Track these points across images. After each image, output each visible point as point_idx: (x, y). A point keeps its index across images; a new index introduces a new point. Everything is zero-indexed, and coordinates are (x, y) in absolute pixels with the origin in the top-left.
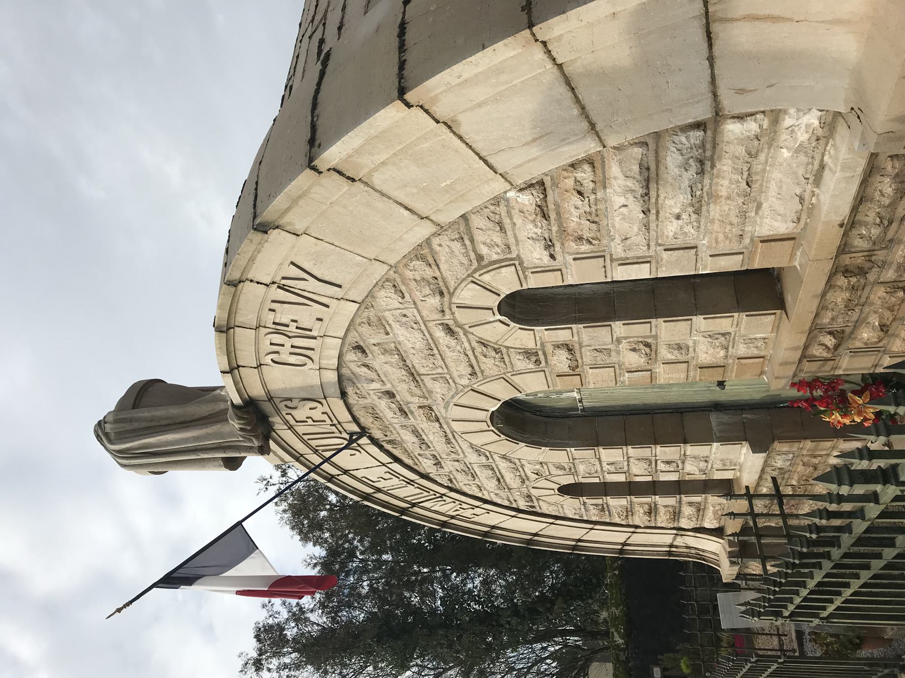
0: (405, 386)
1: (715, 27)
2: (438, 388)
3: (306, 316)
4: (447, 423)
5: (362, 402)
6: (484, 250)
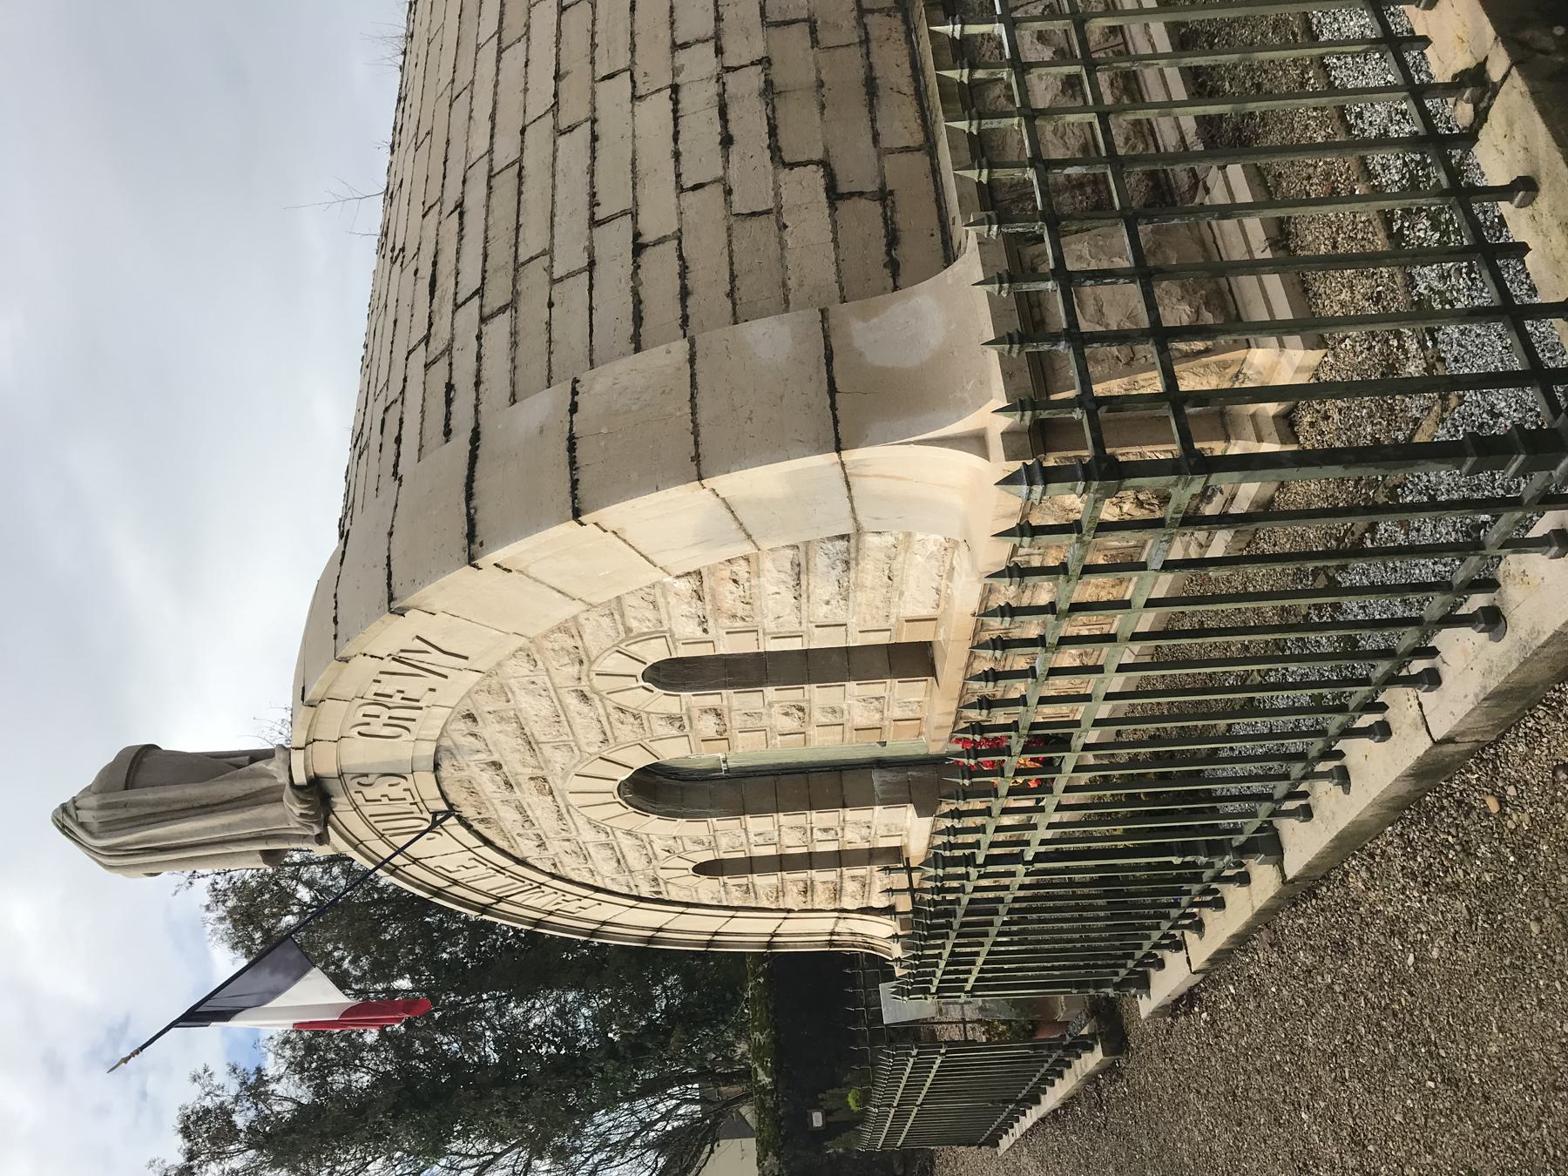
0: (518, 756)
2: (559, 758)
3: (414, 687)
4: (563, 797)
5: (459, 775)
6: (634, 624)
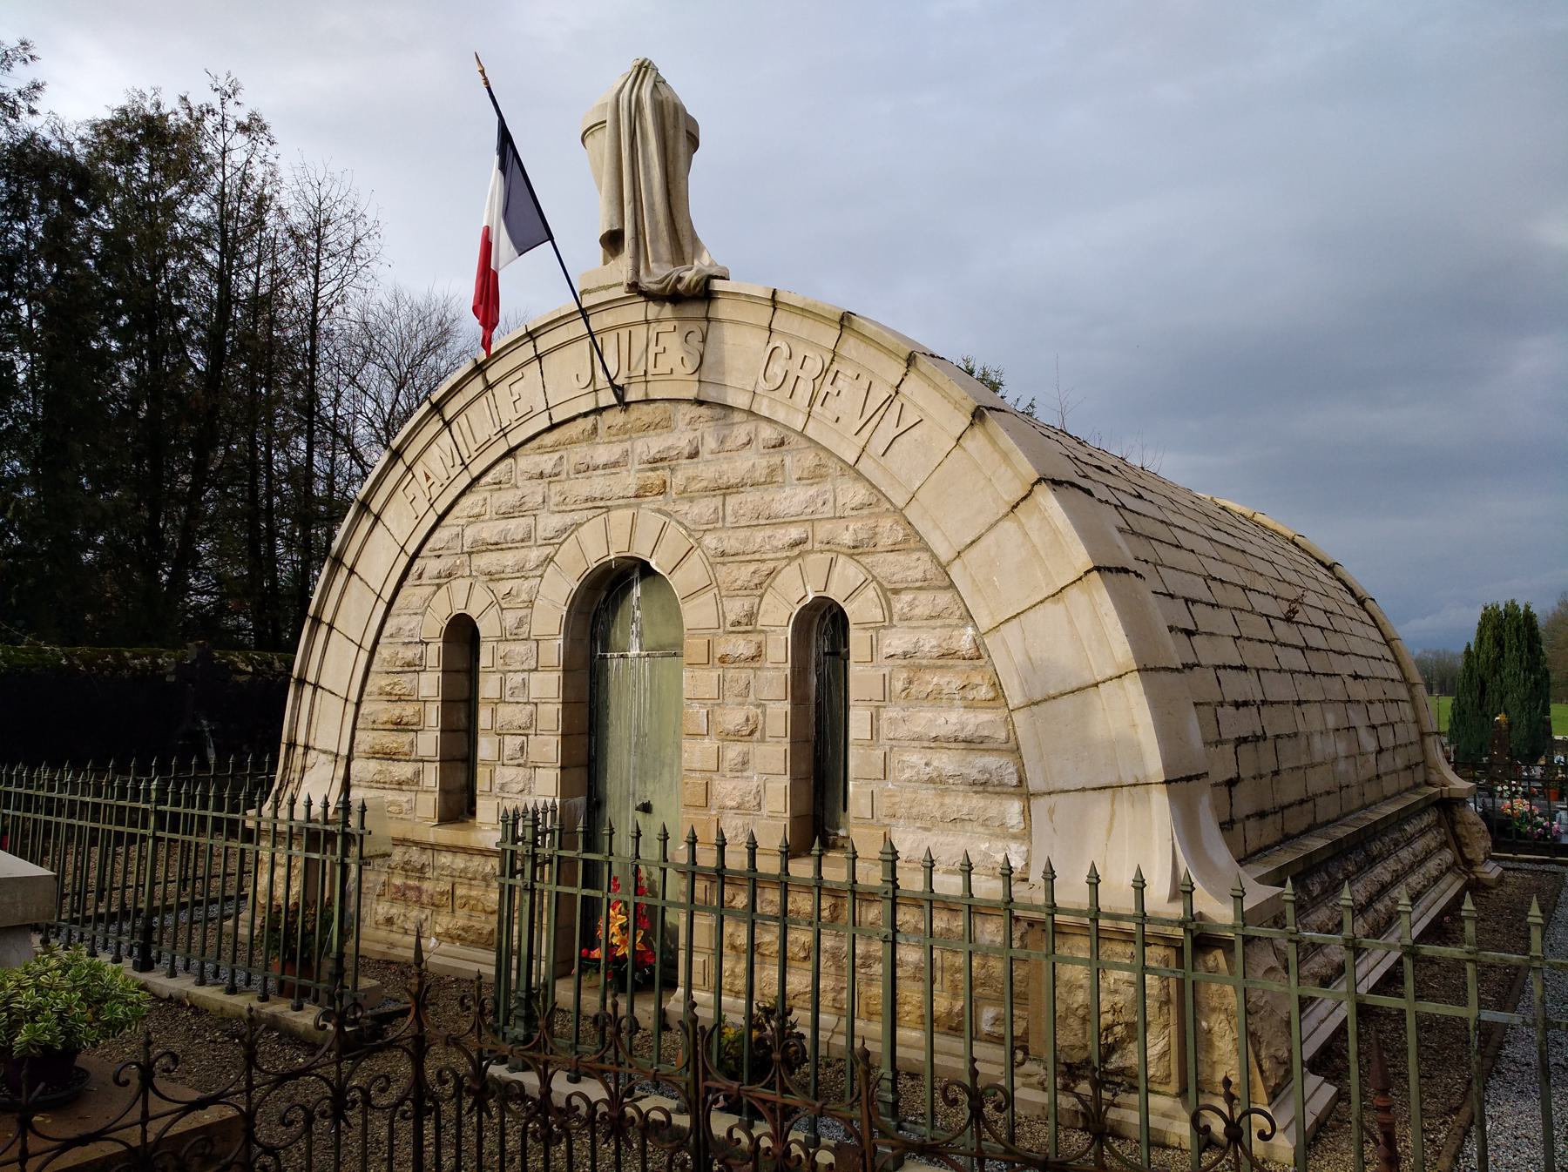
1: (1109, 791)
6: (906, 597)
